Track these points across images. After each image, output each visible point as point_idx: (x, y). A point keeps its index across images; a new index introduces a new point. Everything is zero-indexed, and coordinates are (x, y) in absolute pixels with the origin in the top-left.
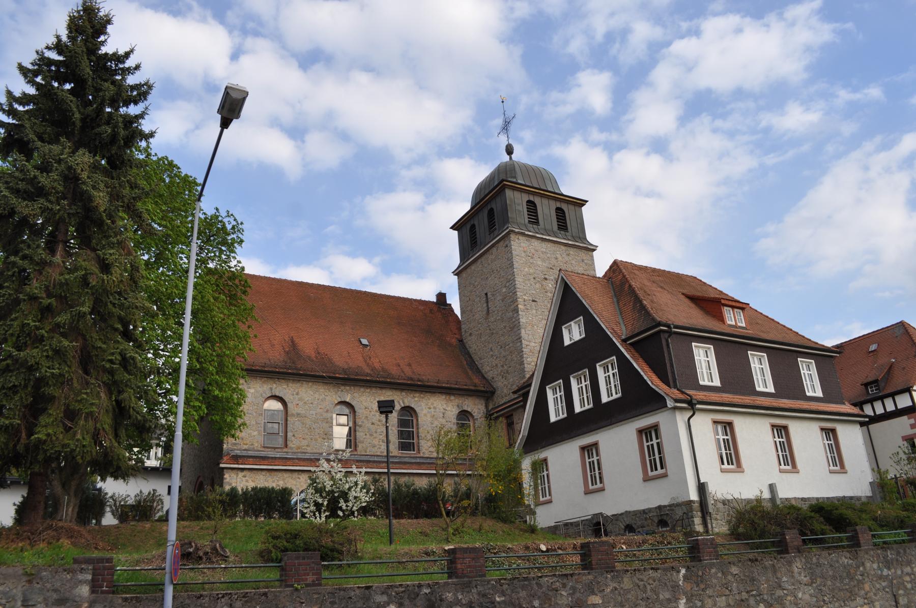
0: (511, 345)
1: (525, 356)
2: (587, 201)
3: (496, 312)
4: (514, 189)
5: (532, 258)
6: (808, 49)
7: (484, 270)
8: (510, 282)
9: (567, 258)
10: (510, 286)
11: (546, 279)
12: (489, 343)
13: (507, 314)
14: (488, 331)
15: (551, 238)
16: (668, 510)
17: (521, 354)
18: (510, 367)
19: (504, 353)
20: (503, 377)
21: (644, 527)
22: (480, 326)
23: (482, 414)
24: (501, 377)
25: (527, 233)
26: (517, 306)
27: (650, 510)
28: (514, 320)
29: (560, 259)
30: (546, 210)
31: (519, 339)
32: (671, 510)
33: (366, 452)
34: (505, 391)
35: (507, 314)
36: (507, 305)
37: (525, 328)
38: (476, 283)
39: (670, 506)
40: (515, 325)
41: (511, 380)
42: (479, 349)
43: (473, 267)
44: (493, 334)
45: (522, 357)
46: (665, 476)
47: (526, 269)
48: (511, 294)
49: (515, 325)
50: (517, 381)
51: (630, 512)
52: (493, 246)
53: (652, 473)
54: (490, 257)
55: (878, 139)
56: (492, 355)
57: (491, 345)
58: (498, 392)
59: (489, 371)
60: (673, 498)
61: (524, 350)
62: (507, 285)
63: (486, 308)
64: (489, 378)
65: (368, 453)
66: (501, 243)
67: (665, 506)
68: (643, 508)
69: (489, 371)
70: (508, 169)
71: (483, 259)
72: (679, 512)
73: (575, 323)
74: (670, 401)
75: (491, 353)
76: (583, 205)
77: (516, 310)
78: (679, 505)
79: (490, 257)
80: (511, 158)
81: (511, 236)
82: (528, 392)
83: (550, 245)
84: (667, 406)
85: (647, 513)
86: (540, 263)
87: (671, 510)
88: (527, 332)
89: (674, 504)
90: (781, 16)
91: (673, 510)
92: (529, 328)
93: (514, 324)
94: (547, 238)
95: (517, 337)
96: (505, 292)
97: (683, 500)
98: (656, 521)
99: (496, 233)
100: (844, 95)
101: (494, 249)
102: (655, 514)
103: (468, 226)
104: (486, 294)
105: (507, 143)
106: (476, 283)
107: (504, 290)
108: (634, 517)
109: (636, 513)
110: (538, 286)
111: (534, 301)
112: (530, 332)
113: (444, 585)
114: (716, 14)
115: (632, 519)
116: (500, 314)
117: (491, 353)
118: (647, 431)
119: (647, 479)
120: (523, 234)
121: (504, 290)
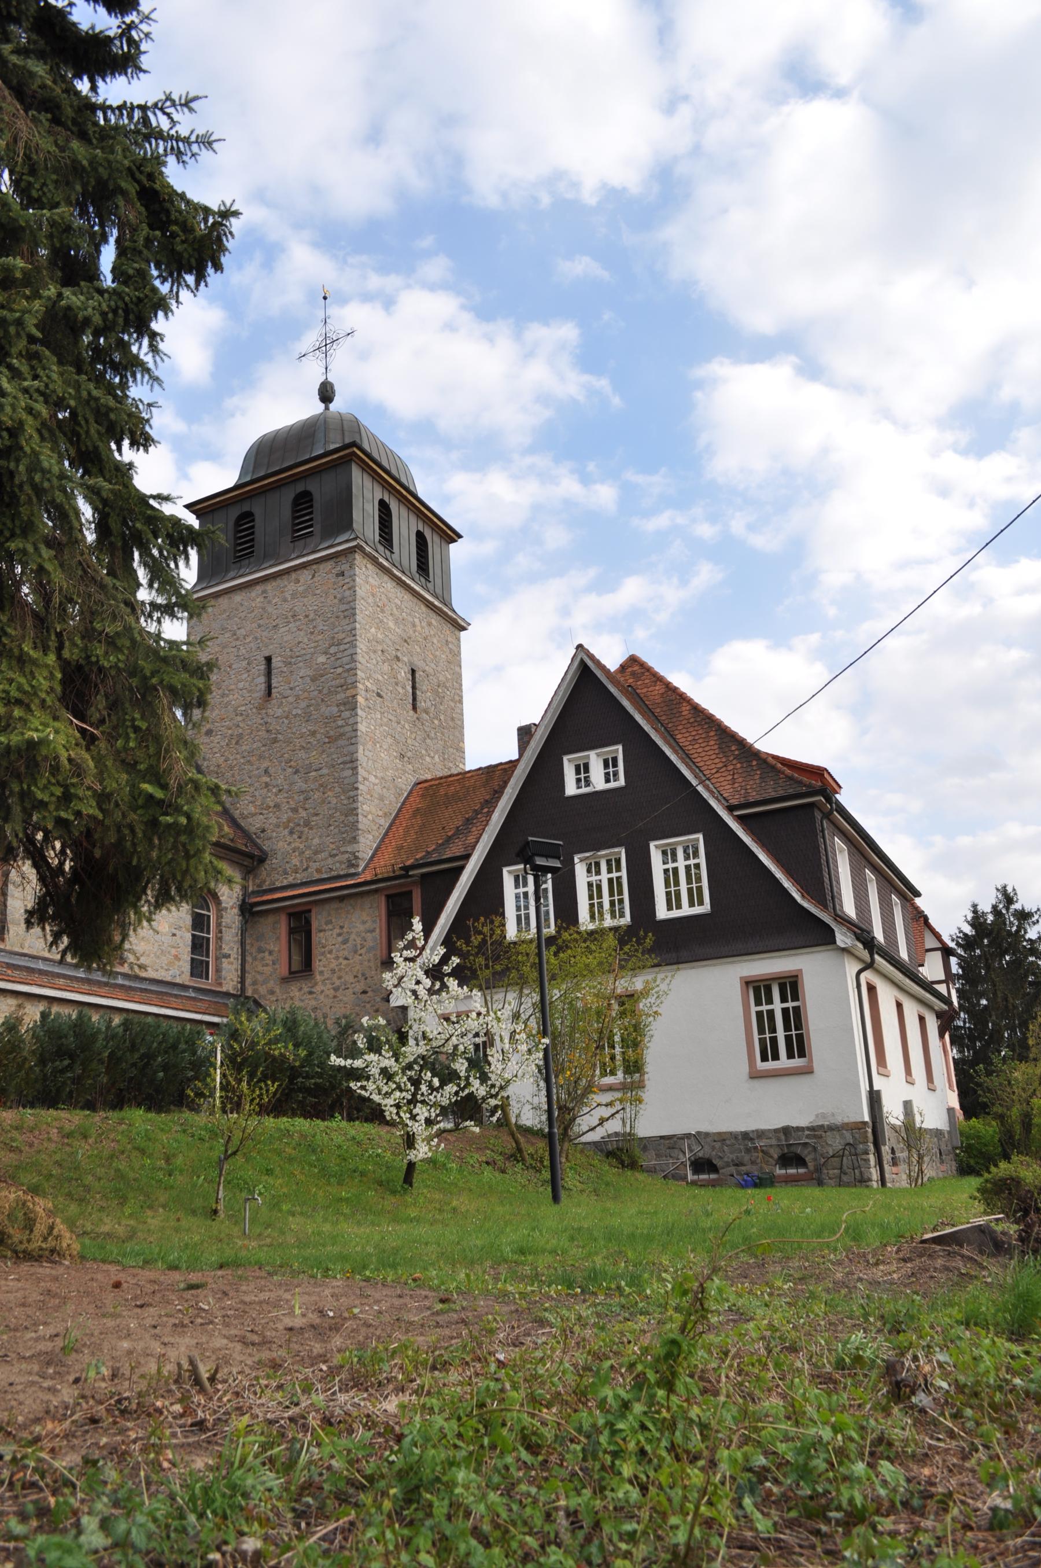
0: (325, 771)
1: (360, 798)
2: (460, 536)
3: (291, 699)
4: (365, 468)
5: (383, 611)
6: (544, 399)
7: (270, 610)
8: (342, 647)
9: (426, 631)
10: (339, 655)
11: (398, 658)
12: (261, 757)
13: (323, 708)
14: (263, 733)
15: (413, 585)
16: (808, 1137)
17: (352, 794)
18: (317, 815)
19: (301, 785)
20: (291, 833)
21: (743, 1165)
22: (239, 718)
23: (234, 900)
24: (286, 832)
25: (381, 560)
26: (354, 696)
27: (761, 1134)
28: (340, 723)
29: (419, 628)
30: (404, 526)
31: (352, 763)
32: (815, 1136)
33: (22, 947)
34: (295, 861)
35: (323, 708)
36: (325, 691)
37: (364, 745)
38: (243, 632)
39: (812, 1129)
40: (342, 735)
41: (316, 841)
42: (231, 768)
43: (238, 598)
44: (275, 741)
45: (354, 799)
46: (808, 1071)
47: (373, 630)
48: (339, 670)
49: (342, 735)
50: (332, 846)
51: (707, 1134)
52: (295, 568)
53: (765, 1064)
54: (289, 586)
55: (592, 572)
56: (267, 785)
57: (266, 764)
58: (273, 862)
59: (254, 815)
60: (824, 1116)
61: (361, 787)
62: (332, 650)
63: (263, 687)
64: (253, 829)
65: (25, 951)
66: (329, 565)
67: (798, 1129)
68: (743, 1128)
69: (254, 815)
70: (346, 427)
71: (269, 586)
72: (835, 1143)
73: (598, 755)
74: (844, 934)
75: (266, 779)
76: (454, 541)
77: (351, 705)
78: (832, 1128)
79: (291, 587)
80: (327, 408)
81: (357, 556)
82: (462, 868)
83: (407, 596)
84: (835, 942)
85: (752, 1139)
86: (391, 625)
87: (815, 1136)
88: (367, 753)
89: (822, 1126)
90: (518, 335)
91: (821, 1137)
92: (369, 746)
93: (342, 730)
94: (408, 581)
95: (348, 758)
96: (323, 664)
97: (846, 1120)
98: (776, 1156)
99: (312, 542)
100: (569, 486)
101: (305, 575)
102: (774, 1142)
103: (234, 513)
104: (268, 660)
105: (322, 379)
106: (243, 632)
107: (322, 659)
108: (718, 1145)
109: (722, 1138)
110: (386, 667)
111: (379, 695)
112: (370, 754)
113: (822, 1231)
114: (432, 287)
115: (713, 1148)
116: (303, 705)
117: (266, 779)
118: (762, 984)
119: (755, 1075)
120: (374, 561)
121: (322, 659)
